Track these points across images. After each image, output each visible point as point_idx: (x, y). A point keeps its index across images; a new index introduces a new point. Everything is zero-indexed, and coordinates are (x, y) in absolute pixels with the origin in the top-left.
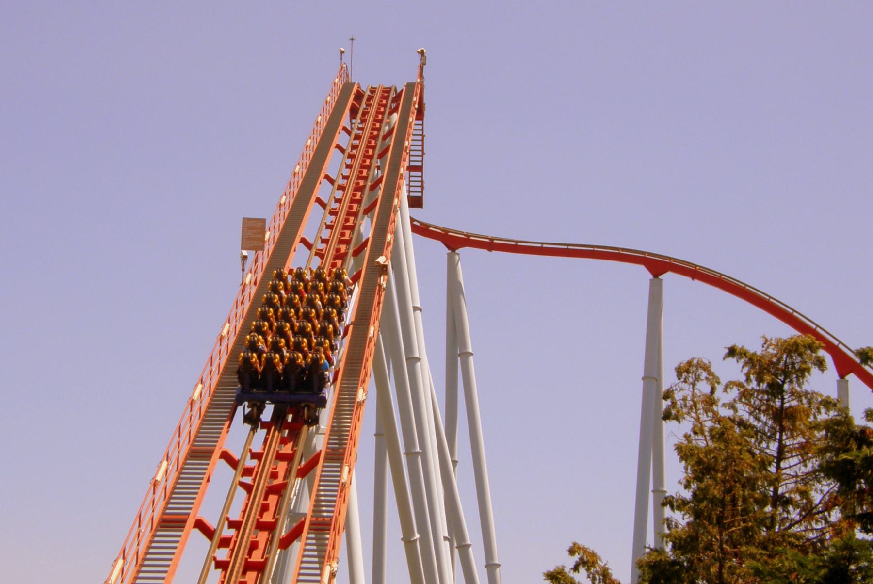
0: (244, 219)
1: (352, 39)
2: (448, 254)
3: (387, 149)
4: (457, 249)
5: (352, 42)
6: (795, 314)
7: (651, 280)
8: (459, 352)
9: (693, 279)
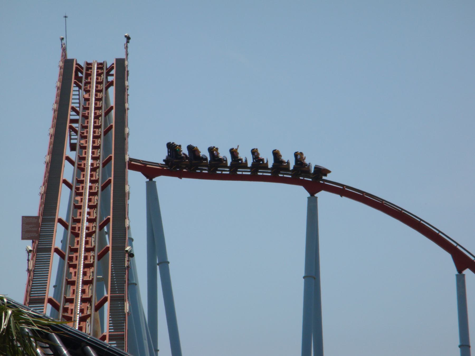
0: (23, 217)
1: (66, 17)
2: (147, 182)
3: (109, 181)
4: (154, 177)
5: (65, 15)
6: (422, 222)
7: (308, 198)
8: (157, 262)
9: (341, 196)
